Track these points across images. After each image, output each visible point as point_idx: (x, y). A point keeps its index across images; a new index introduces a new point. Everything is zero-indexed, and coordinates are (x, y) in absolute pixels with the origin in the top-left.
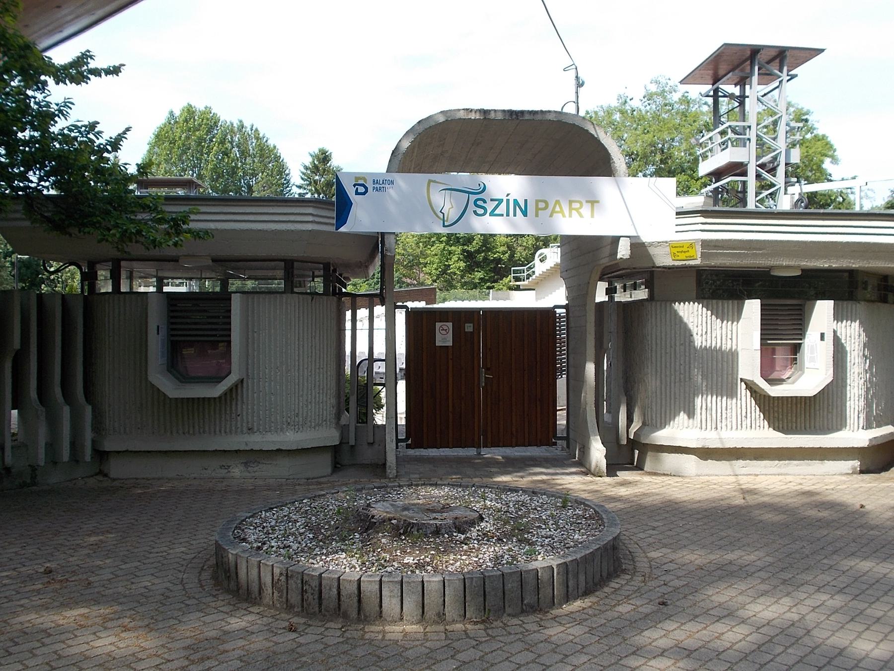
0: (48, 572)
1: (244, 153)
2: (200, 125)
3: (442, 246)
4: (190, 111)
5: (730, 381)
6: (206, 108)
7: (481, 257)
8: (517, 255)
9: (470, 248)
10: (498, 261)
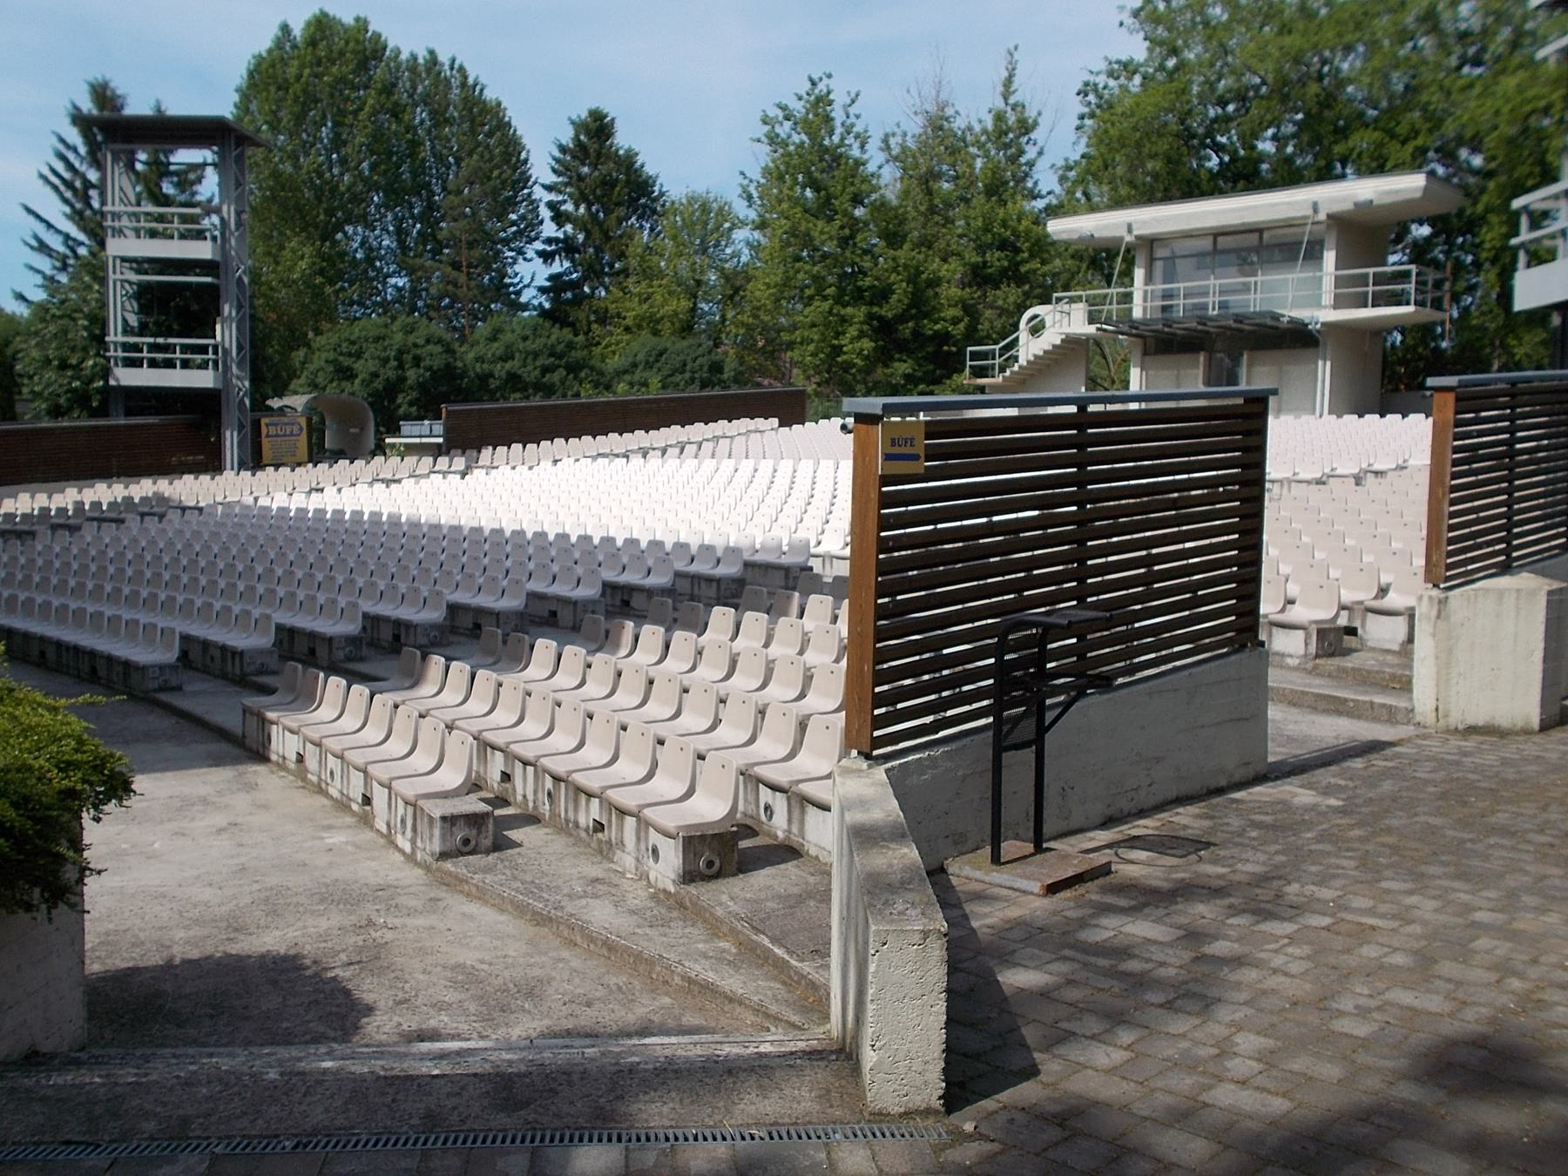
1: (439, 118)
2: (342, 53)
3: (826, 305)
4: (322, 26)
6: (357, 19)
8: (984, 327)
9: (887, 311)
10: (944, 337)
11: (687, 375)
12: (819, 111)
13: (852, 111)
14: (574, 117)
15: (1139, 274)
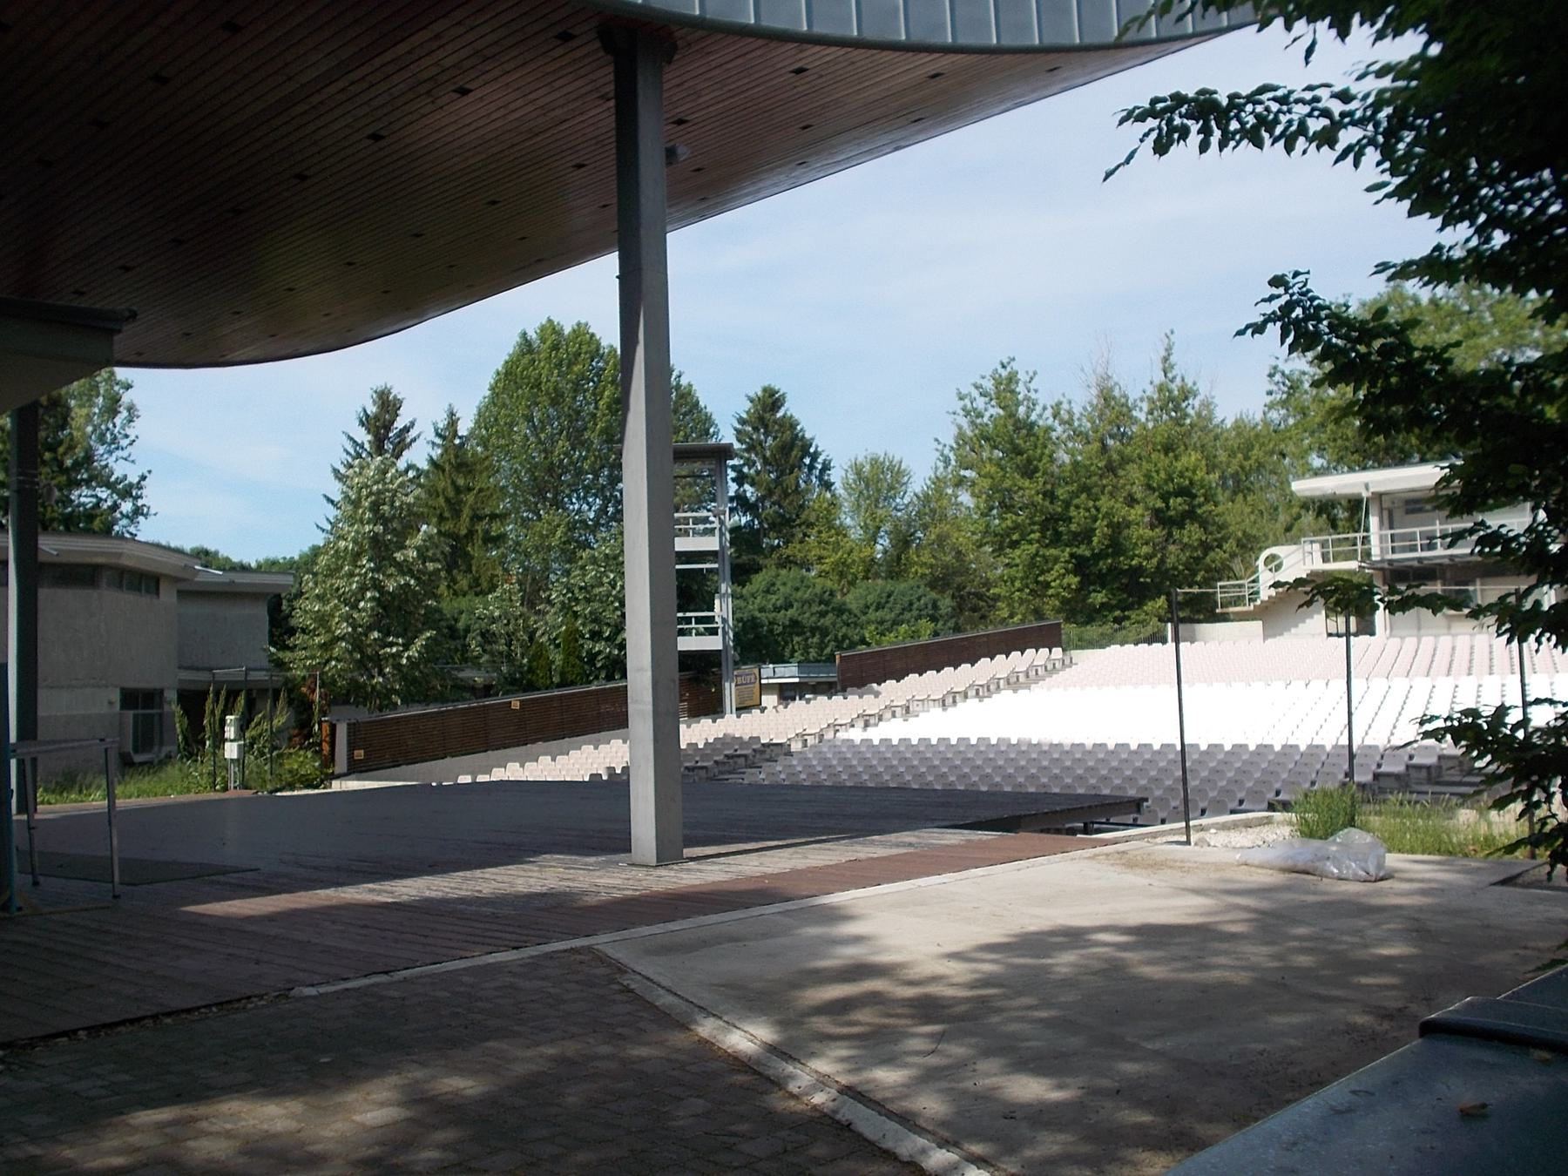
0: (257, 963)
5: (423, 111)
7: (1103, 565)
9: (1083, 551)
10: (1139, 570)
11: (915, 613)
12: (1005, 388)
13: (1032, 386)
14: (752, 394)
15: (1374, 521)
